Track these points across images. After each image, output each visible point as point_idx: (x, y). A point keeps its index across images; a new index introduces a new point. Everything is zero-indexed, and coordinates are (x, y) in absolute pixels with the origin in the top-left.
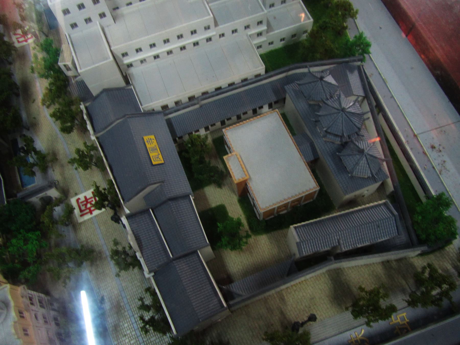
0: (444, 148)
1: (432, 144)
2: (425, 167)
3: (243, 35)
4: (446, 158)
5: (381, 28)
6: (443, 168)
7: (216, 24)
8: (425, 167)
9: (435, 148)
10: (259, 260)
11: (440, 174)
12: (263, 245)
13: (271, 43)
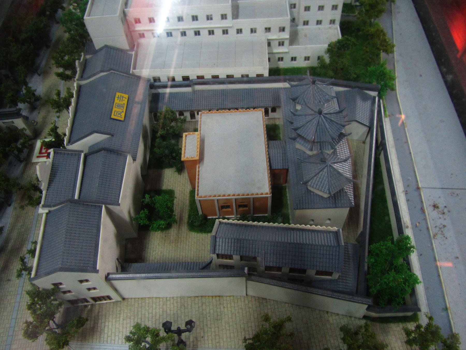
0: (449, 212)
1: (437, 203)
2: (418, 224)
3: (261, 36)
4: (447, 222)
5: (421, 76)
6: (440, 232)
7: (236, 16)
8: (418, 224)
9: (438, 207)
10: (181, 257)
11: (434, 238)
12: (193, 243)
13: (294, 59)
